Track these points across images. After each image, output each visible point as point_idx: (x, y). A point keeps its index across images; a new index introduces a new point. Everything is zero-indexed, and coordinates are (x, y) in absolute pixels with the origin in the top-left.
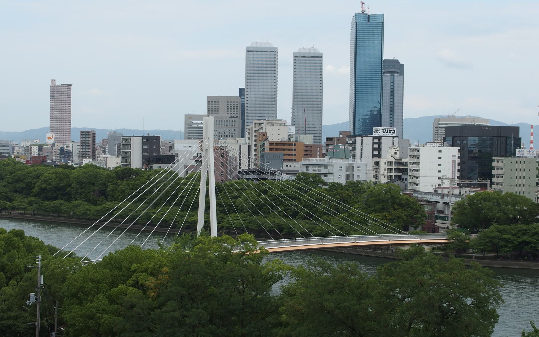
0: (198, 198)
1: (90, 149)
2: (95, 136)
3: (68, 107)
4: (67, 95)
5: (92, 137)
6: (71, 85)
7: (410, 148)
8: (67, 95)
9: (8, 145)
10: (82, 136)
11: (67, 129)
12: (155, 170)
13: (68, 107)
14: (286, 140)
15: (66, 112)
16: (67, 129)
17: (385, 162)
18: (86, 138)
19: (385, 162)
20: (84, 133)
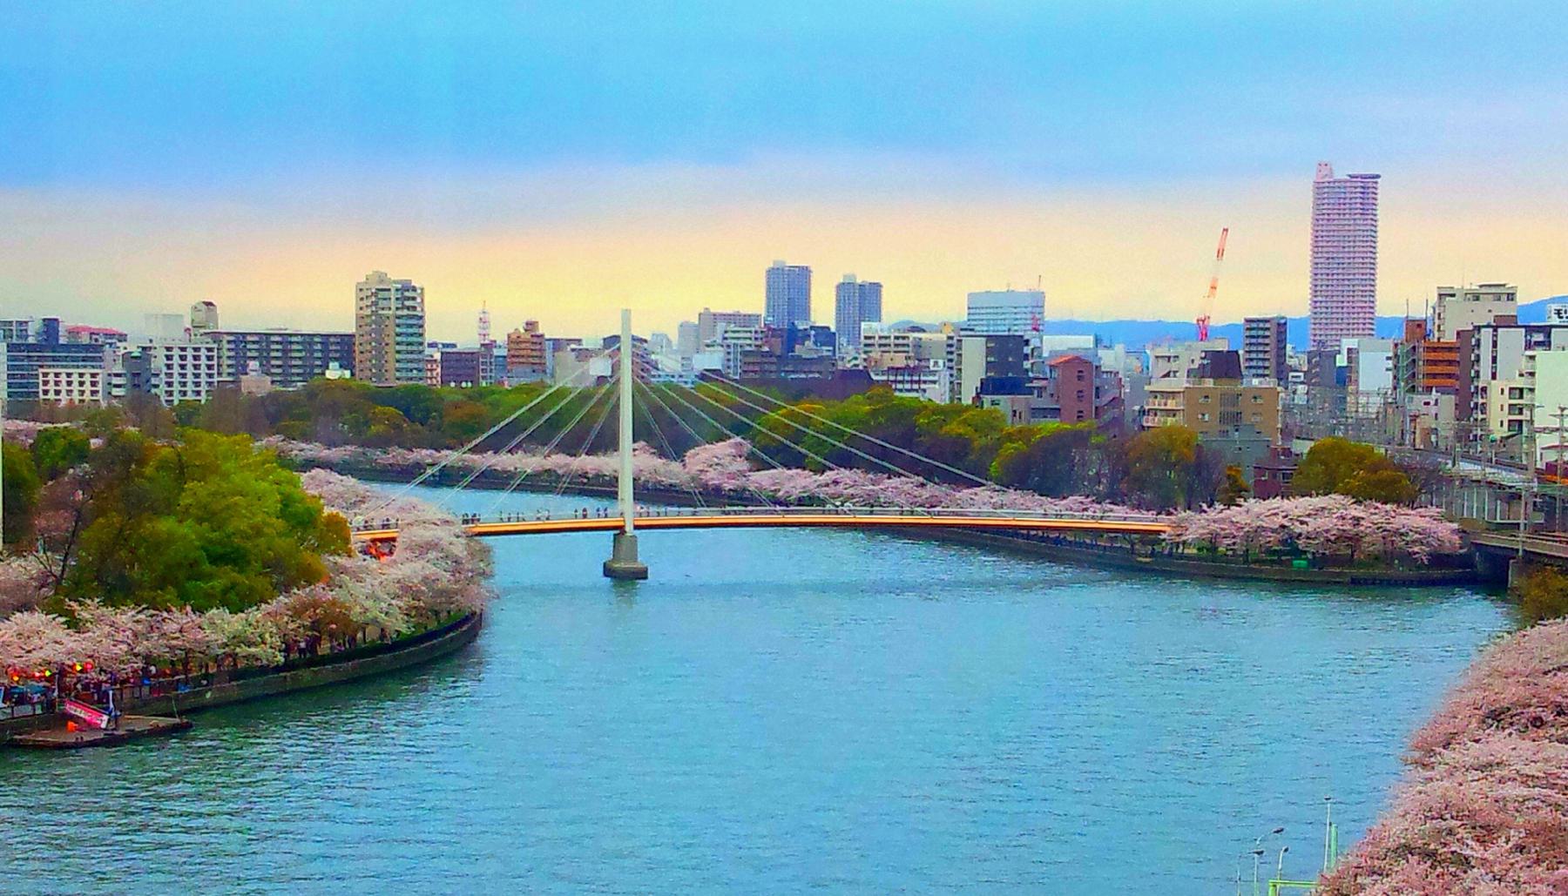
0: (617, 407)
1: (1268, 359)
2: (629, 320)
3: (1361, 244)
4: (1361, 201)
5: (1275, 341)
6: (1378, 176)
7: (1147, 388)
8: (1361, 201)
9: (1452, 292)
10: (1248, 333)
11: (1360, 310)
12: (248, 365)
13: (1361, 244)
14: (31, 340)
15: (1356, 260)
16: (1360, 310)
17: (1502, 406)
18: (1258, 337)
19: (1502, 406)
20: (1254, 325)
